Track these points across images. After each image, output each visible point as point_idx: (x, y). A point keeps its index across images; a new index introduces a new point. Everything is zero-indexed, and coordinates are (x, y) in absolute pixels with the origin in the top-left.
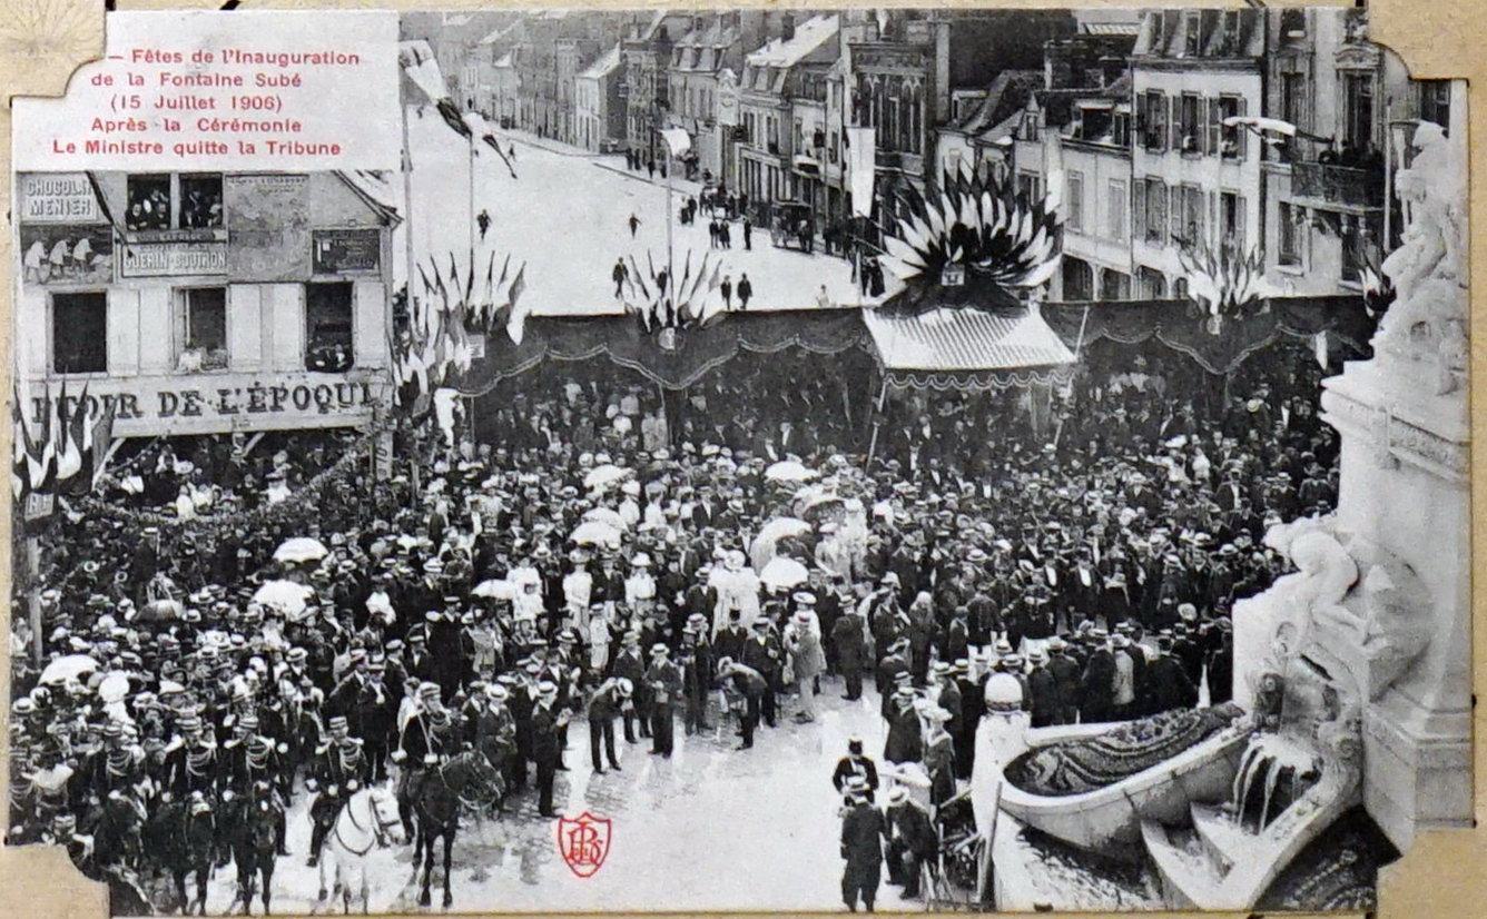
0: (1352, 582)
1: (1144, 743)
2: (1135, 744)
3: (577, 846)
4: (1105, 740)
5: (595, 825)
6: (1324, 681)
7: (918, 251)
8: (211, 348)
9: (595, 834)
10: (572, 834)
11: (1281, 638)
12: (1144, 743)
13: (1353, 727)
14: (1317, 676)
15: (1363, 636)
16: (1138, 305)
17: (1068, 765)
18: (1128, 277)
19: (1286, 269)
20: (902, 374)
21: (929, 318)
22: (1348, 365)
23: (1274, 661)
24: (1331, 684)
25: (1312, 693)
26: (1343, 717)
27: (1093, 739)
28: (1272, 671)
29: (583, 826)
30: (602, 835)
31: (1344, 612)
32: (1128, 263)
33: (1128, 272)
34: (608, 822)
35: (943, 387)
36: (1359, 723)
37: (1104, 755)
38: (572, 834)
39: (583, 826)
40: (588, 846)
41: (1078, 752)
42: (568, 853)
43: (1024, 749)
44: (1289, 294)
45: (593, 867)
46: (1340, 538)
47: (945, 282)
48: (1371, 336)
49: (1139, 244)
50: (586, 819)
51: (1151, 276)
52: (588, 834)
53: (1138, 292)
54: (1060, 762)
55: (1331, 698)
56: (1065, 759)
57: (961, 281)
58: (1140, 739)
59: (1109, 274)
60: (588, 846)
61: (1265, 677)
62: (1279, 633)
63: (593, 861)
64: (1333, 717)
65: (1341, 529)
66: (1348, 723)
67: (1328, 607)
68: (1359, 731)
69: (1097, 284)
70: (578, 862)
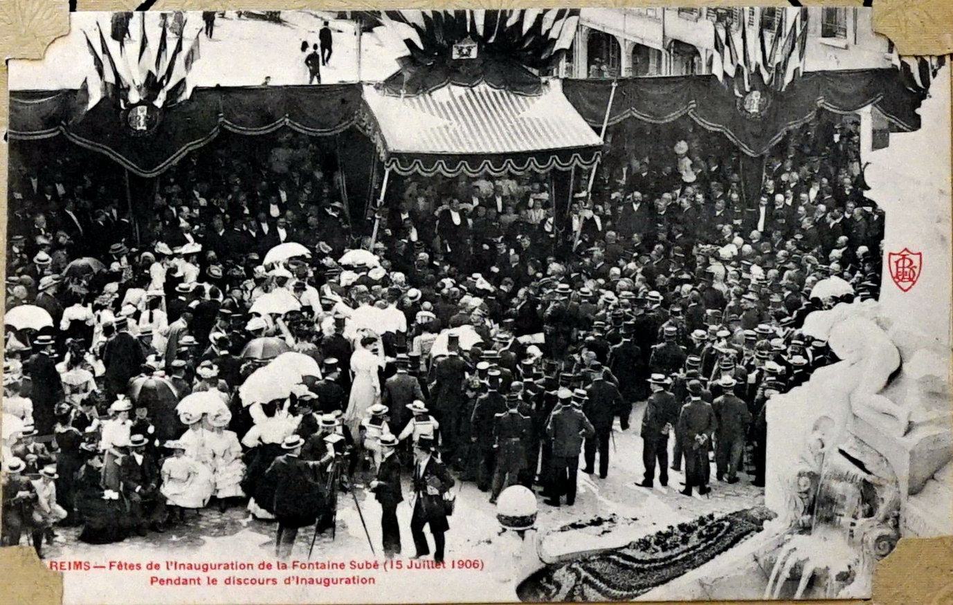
0: (894, 368)
1: (669, 553)
2: (661, 555)
3: (900, 270)
4: (628, 552)
5: (911, 256)
6: (862, 475)
7: (414, 26)
8: (444, 27)
9: (911, 262)
10: (897, 262)
11: (818, 435)
12: (669, 553)
13: (890, 523)
14: (855, 470)
15: (904, 424)
16: (668, 80)
17: (586, 580)
18: (659, 51)
19: (828, 41)
20: (406, 158)
21: (442, 95)
22: (894, 137)
23: (810, 458)
24: (869, 478)
25: (846, 491)
26: (882, 510)
27: (614, 551)
28: (809, 469)
29: (904, 257)
30: (916, 263)
31: (884, 402)
32: (660, 38)
33: (659, 47)
34: (920, 254)
35: (448, 174)
36: (897, 518)
37: (625, 567)
38: (897, 262)
39: (904, 257)
40: (907, 270)
41: (597, 566)
42: (894, 274)
43: (536, 566)
44: (832, 66)
45: (911, 283)
46: (882, 325)
47: (455, 56)
48: (919, 105)
49: (671, 17)
50: (905, 253)
51: (683, 50)
52: (907, 263)
53: (669, 68)
54: (578, 578)
55: (868, 493)
56: (584, 574)
57: (474, 54)
58: (664, 549)
59: (640, 51)
60: (907, 270)
61: (800, 475)
62: (815, 428)
63: (910, 279)
64: (870, 514)
65: (883, 315)
66: (886, 519)
67: (868, 396)
68: (896, 526)
69: (625, 63)
70: (901, 280)
